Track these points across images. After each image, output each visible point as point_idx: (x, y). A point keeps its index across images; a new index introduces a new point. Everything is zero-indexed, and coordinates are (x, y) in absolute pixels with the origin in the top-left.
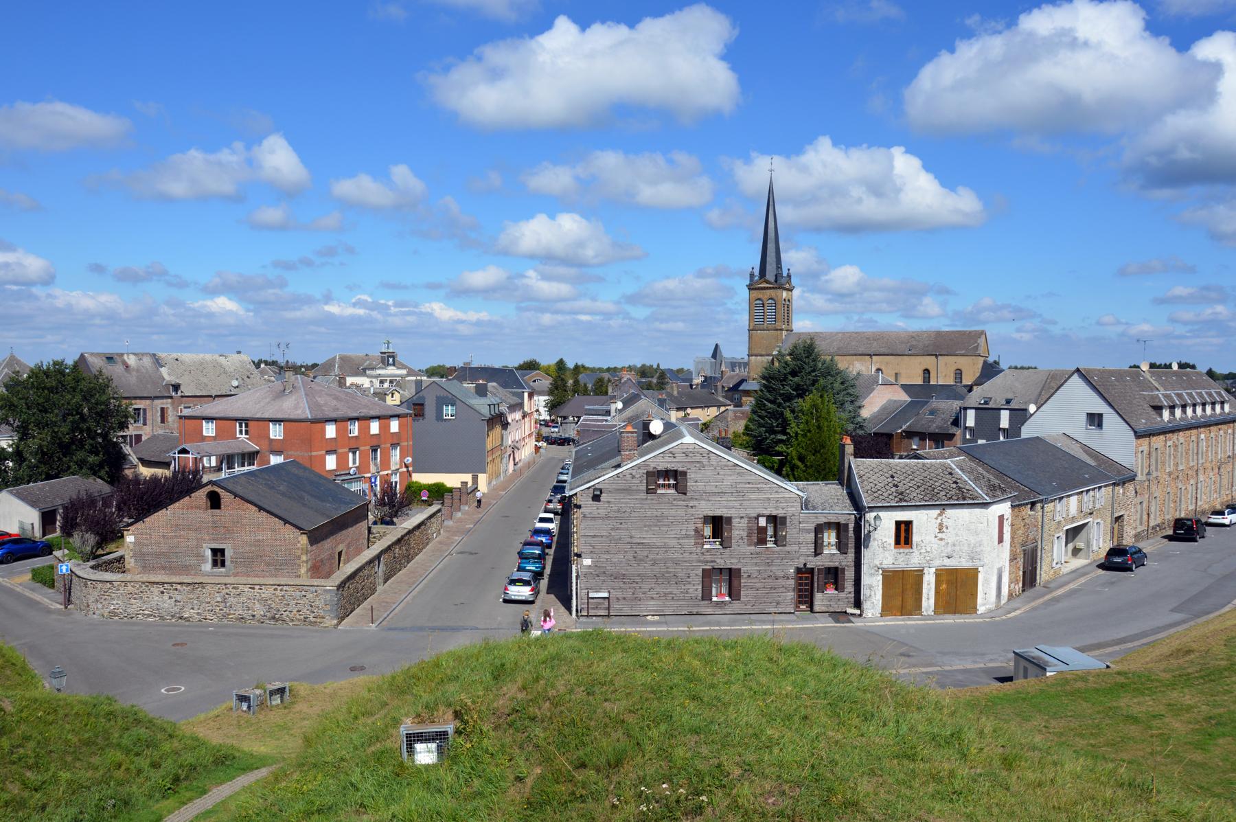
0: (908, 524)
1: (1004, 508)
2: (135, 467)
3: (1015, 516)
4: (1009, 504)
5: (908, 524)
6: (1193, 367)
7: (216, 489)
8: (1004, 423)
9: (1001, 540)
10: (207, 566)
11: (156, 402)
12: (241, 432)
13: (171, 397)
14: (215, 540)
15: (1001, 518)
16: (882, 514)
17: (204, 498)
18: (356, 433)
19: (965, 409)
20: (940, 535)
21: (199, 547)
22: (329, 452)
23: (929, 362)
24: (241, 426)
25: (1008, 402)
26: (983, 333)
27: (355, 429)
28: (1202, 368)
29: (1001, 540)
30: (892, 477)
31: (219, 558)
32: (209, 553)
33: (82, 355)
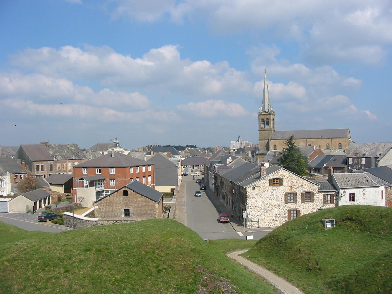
0: (353, 194)
1: (382, 188)
2: (49, 186)
3: (386, 191)
4: (384, 186)
5: (353, 194)
6: (195, 147)
7: (126, 189)
8: (363, 162)
9: (382, 199)
10: (123, 216)
11: (48, 162)
12: (98, 172)
13: (53, 161)
14: (126, 206)
15: (382, 191)
16: (346, 190)
17: (122, 192)
18: (139, 172)
19: (348, 158)
20: (364, 197)
21: (120, 209)
22: (149, 176)
23: (329, 141)
24: (98, 170)
25: (364, 155)
26: (348, 129)
27: (138, 171)
28: (158, 145)
29: (382, 199)
30: (347, 179)
31: (127, 213)
32: (124, 211)
33: (21, 145)
